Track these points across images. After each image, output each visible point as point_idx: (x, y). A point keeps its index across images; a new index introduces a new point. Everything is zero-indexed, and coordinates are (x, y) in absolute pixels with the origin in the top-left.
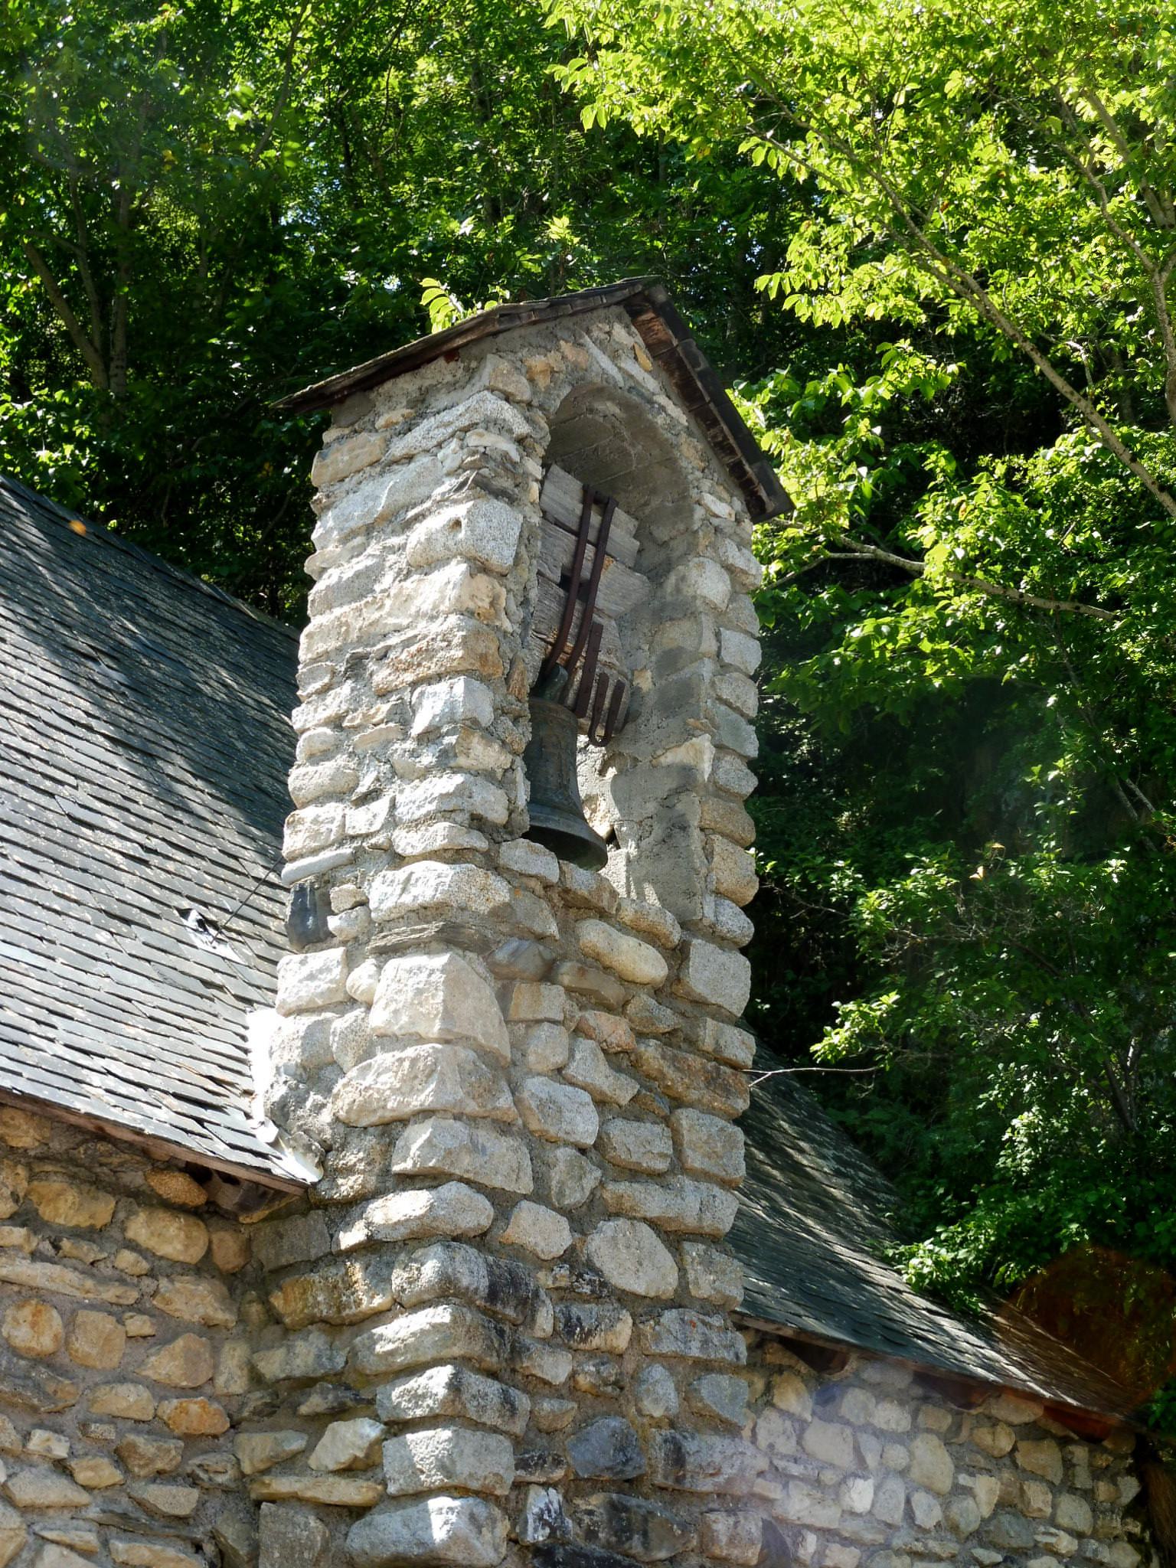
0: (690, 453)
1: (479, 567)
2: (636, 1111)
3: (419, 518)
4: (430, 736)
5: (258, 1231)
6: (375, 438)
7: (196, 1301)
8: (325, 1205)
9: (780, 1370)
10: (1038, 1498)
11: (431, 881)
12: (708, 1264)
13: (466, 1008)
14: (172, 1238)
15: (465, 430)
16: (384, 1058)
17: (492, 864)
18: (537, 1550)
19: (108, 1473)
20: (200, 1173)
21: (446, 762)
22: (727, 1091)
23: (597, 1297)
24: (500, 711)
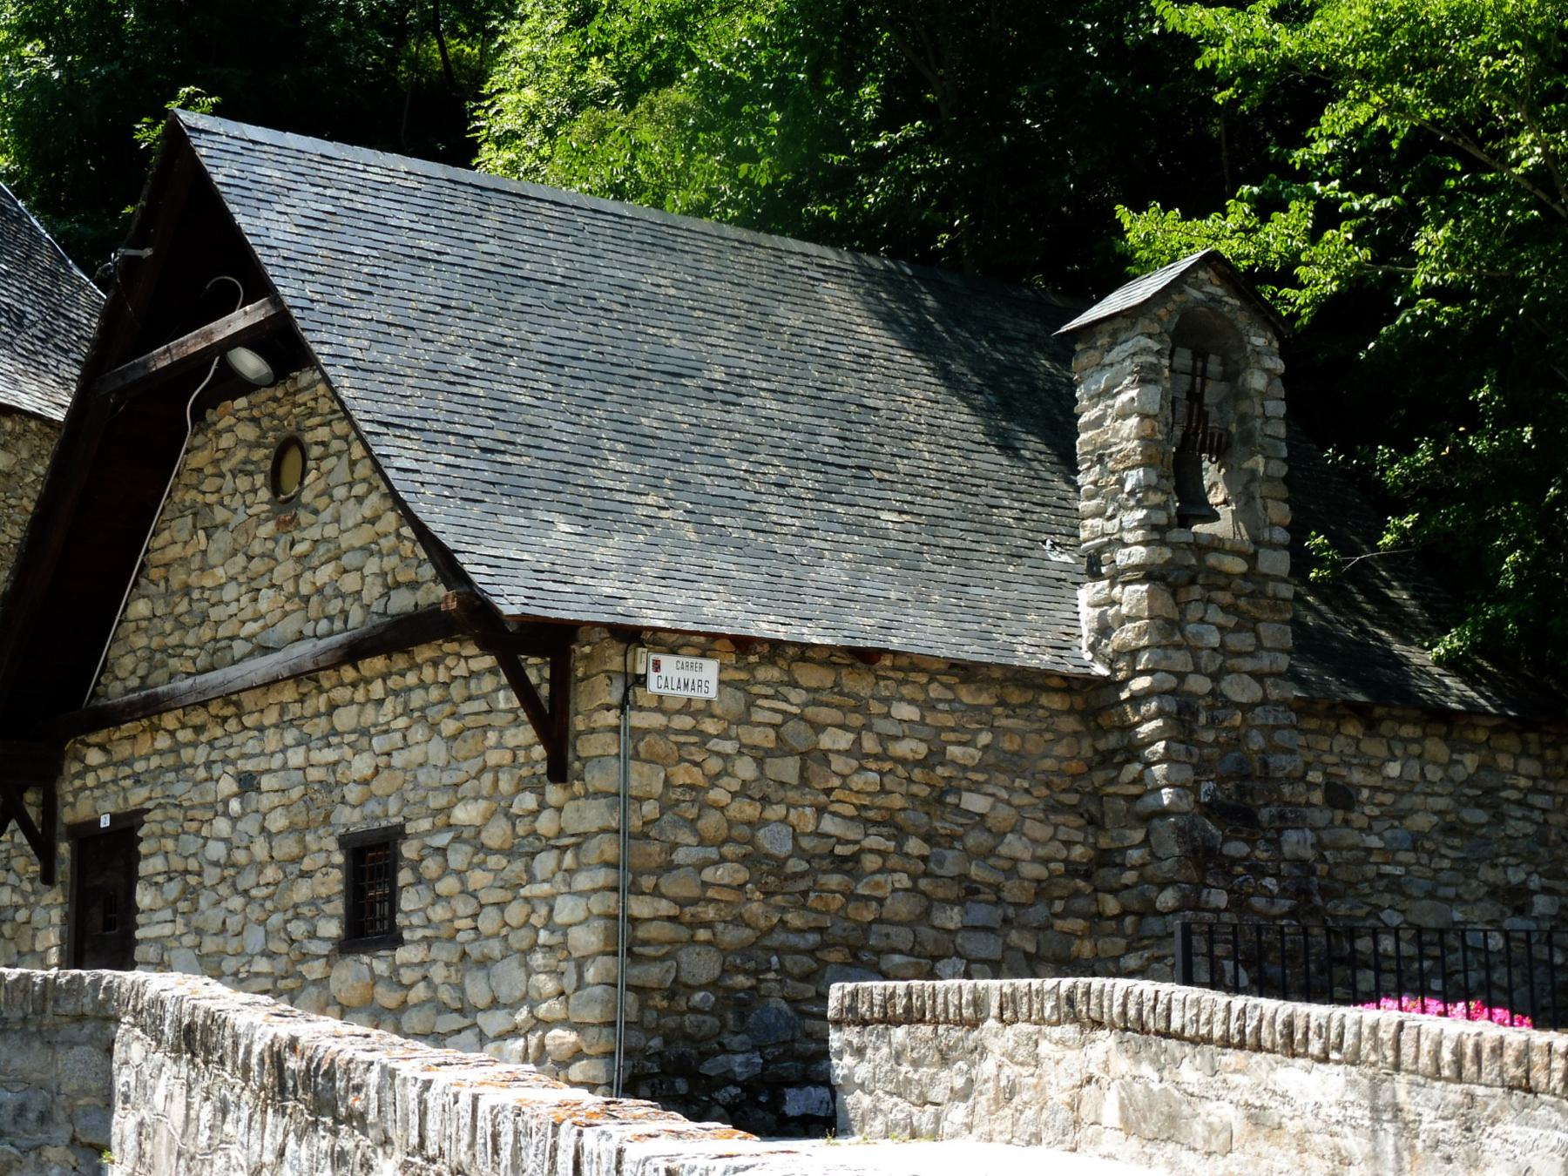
0: (1242, 320)
1: (1144, 416)
2: (1238, 629)
3: (1119, 393)
4: (1132, 493)
5: (1091, 699)
6: (1097, 354)
7: (1069, 724)
8: (1115, 683)
9: (1344, 716)
10: (1505, 761)
11: (1138, 554)
12: (1276, 686)
13: (1158, 604)
14: (1057, 702)
15: (1134, 354)
16: (1128, 626)
17: (1162, 543)
18: (1205, 804)
19: (1045, 792)
20: (1064, 677)
21: (1140, 504)
22: (1280, 612)
23: (1224, 707)
24: (1160, 477)
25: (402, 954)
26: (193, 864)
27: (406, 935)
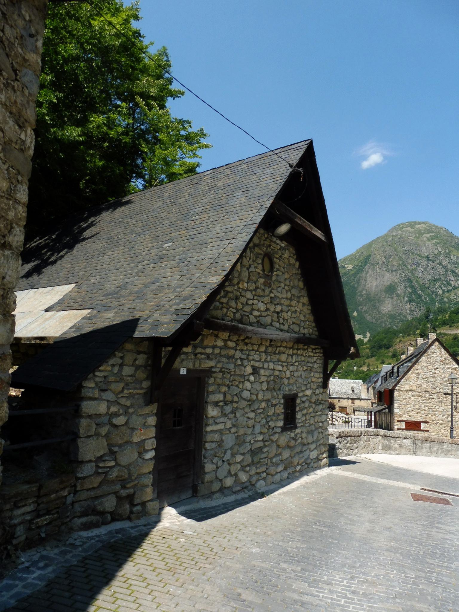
25: (298, 431)
26: (236, 399)
27: (298, 425)
